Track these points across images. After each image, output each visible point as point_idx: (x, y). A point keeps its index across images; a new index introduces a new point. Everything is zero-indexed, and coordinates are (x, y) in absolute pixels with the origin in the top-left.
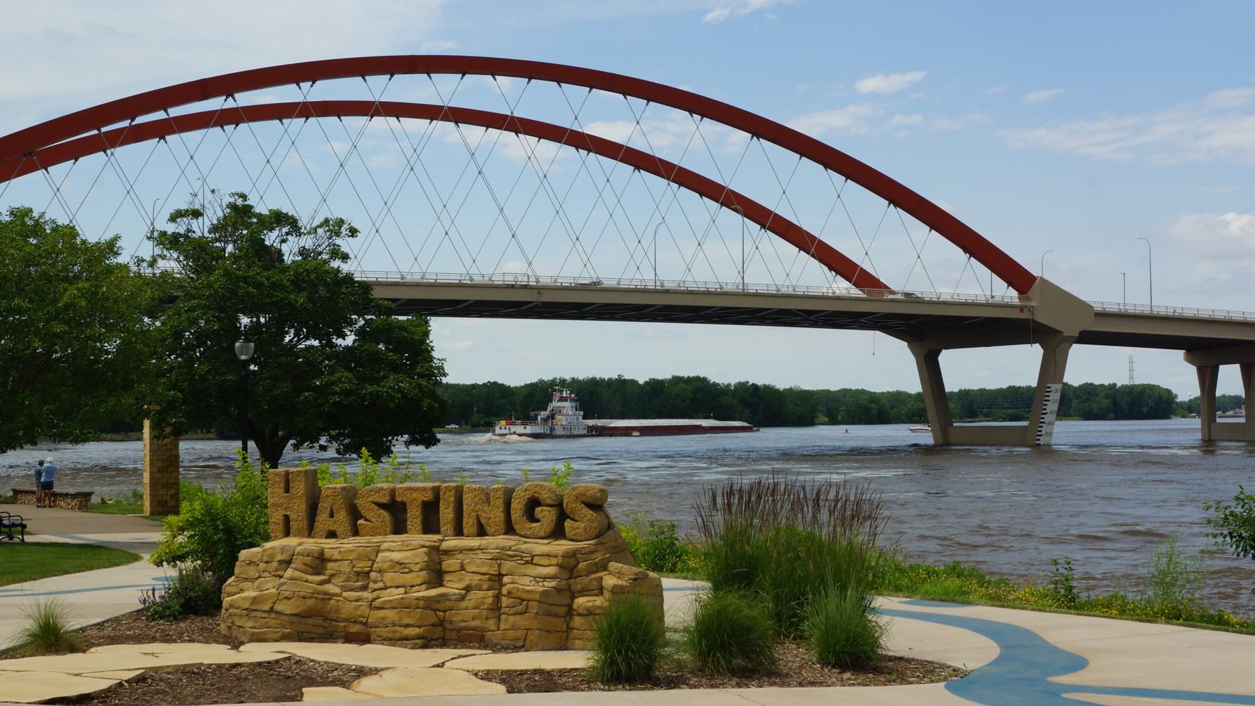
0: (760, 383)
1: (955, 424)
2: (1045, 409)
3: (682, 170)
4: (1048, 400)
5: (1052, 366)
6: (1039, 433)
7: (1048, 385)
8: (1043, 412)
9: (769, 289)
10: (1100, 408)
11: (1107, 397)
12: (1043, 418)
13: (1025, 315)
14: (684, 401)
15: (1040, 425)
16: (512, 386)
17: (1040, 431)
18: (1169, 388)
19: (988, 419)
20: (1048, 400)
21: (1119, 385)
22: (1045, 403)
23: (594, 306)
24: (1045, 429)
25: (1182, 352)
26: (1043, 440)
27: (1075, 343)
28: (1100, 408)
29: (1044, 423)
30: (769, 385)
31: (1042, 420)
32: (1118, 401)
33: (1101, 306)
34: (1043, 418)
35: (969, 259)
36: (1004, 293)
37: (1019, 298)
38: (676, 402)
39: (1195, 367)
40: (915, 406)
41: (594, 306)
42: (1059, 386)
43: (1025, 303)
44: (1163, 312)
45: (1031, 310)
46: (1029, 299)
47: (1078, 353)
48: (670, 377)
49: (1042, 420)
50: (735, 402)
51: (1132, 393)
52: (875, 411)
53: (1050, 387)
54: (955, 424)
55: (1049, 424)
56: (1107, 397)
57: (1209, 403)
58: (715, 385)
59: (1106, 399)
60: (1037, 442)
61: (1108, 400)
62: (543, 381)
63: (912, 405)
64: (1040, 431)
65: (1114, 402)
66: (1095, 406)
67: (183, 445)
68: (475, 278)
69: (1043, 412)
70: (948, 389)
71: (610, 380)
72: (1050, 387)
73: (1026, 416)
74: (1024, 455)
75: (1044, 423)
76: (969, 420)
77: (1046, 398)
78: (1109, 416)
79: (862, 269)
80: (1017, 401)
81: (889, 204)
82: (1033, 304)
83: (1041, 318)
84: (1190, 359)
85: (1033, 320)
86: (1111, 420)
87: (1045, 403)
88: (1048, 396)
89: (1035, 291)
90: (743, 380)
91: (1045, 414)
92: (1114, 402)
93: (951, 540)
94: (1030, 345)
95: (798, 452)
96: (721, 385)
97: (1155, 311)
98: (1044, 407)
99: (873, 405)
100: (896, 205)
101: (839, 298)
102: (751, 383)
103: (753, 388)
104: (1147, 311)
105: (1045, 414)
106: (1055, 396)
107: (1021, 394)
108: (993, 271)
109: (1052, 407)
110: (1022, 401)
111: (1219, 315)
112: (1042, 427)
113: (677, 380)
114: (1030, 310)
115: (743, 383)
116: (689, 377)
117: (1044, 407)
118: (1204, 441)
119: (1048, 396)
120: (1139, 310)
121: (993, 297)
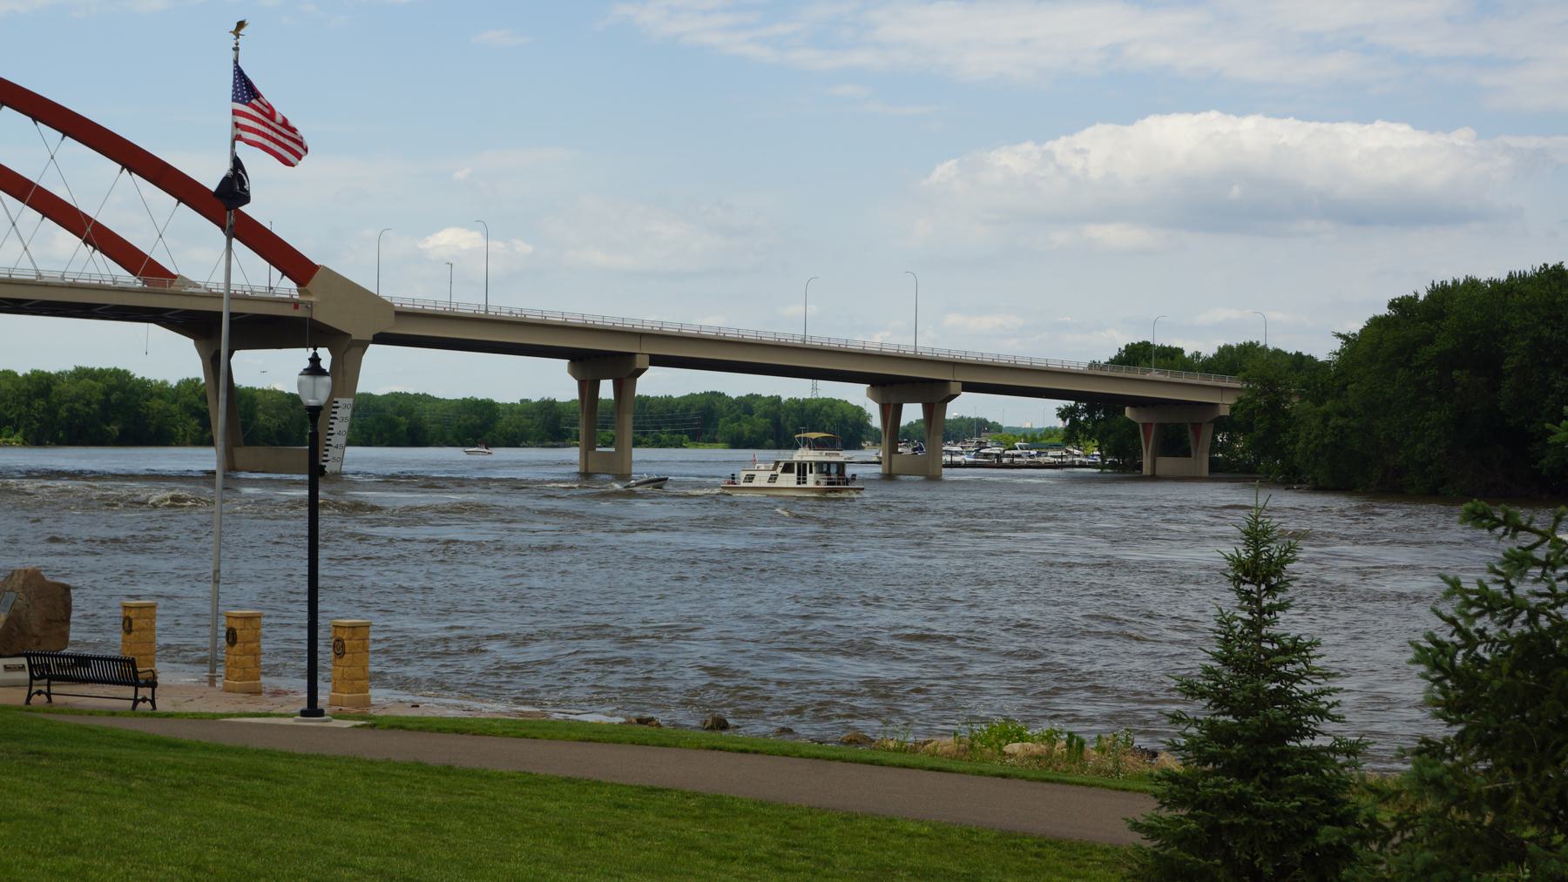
1: (597, 449)
3: (98, 228)
4: (335, 418)
5: (345, 372)
8: (330, 432)
10: (753, 432)
11: (765, 415)
14: (88, 404)
16: (52, 372)
17: (326, 456)
18: (121, 368)
20: (335, 418)
21: (785, 398)
24: (332, 453)
25: (566, 362)
27: (373, 343)
28: (753, 432)
29: (330, 445)
32: (782, 421)
36: (286, 287)
38: (77, 405)
39: (576, 382)
40: (468, 422)
42: (350, 401)
43: (305, 298)
44: (505, 314)
45: (310, 306)
46: (308, 293)
48: (72, 368)
50: (175, 408)
51: (803, 410)
52: (404, 428)
56: (765, 415)
57: (894, 432)
58: (143, 384)
59: (766, 418)
61: (767, 420)
62: (119, 370)
63: (465, 420)
64: (326, 456)
65: (777, 423)
66: (746, 428)
67: (638, 454)
69: (330, 432)
74: (918, 482)
75: (330, 445)
76: (551, 443)
77: (333, 415)
78: (767, 443)
79: (151, 260)
80: (645, 418)
81: (122, 169)
82: (313, 299)
83: (323, 316)
84: (573, 371)
85: (311, 320)
86: (769, 448)
91: (332, 434)
92: (777, 423)
93: (830, 635)
99: (402, 419)
100: (130, 171)
101: (123, 290)
105: (332, 434)
106: (344, 411)
107: (650, 407)
108: (272, 262)
109: (341, 425)
110: (651, 418)
111: (534, 316)
113: (82, 374)
115: (1410, 298)
116: (101, 370)
121: (271, 288)
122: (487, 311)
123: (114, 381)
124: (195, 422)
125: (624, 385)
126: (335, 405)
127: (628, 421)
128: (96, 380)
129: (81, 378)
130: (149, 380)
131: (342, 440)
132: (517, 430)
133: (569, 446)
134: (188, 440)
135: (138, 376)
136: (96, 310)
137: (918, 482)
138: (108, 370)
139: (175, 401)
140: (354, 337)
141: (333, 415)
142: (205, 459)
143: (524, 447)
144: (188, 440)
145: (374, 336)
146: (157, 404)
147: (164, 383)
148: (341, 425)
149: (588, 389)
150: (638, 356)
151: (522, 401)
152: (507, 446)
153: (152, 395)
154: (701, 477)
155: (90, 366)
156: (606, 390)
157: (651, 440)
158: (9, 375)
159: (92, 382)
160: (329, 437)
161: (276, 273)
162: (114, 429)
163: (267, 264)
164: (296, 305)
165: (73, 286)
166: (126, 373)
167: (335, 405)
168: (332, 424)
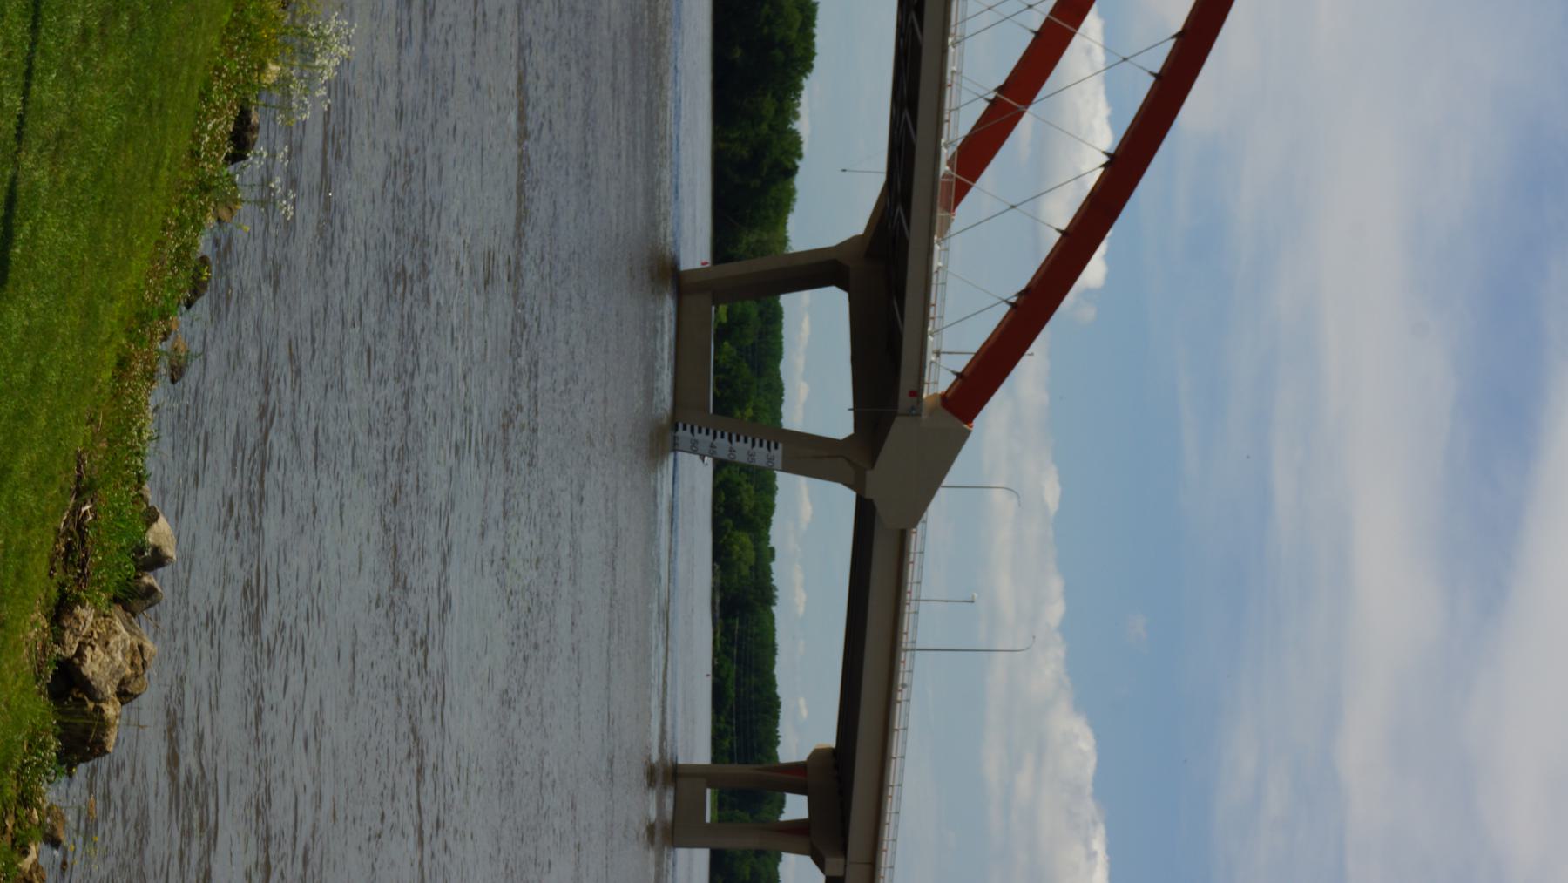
0: (800, 181)
1: (709, 791)
2: (738, 440)
4: (753, 445)
6: (696, 429)
7: (780, 445)
9: (940, 287)
12: (722, 436)
13: (904, 400)
15: (711, 431)
18: (817, 61)
19: (718, 645)
20: (753, 445)
22: (750, 439)
23: (904, 222)
24: (704, 439)
26: (684, 435)
30: (794, 200)
31: (719, 434)
33: (896, 783)
34: (722, 436)
35: (1006, 301)
36: (940, 378)
37: (935, 395)
40: (746, 497)
41: (904, 222)
45: (915, 410)
47: (842, 500)
49: (719, 434)
53: (776, 447)
54: (709, 791)
55: (712, 446)
58: (798, 88)
60: (681, 425)
62: (812, 58)
68: (905, 690)
70: (787, 301)
71: (777, 732)
72: (776, 447)
73: (722, 719)
74: (650, 393)
76: (718, 600)
77: (757, 442)
82: (924, 416)
83: (899, 431)
84: (818, 754)
85: (895, 415)
87: (750, 439)
88: (761, 445)
89: (950, 421)
90: (805, 148)
94: (851, 406)
95: (675, 513)
96: (796, 102)
97: (905, 657)
98: (742, 438)
102: (799, 163)
103: (789, 165)
104: (906, 640)
105: (730, 440)
106: (761, 456)
109: (742, 451)
112: (707, 433)
114: (913, 408)
116: (813, 36)
117: (742, 438)
118: (676, 767)
119: (761, 445)
120: (908, 623)
121: (938, 353)
122: (906, 650)
123: (799, 52)
124: (745, 153)
125: (799, 836)
126: (772, 444)
127: (750, 842)
128: (800, 30)
129: (802, 11)
130: (800, 96)
131: (723, 454)
132: (735, 557)
133: (714, 624)
134: (722, 145)
135: (805, 82)
136: (906, 114)
137: (650, 393)
138: (813, 45)
139: (771, 127)
140: (869, 473)
141: (757, 442)
142: (695, 251)
143: (713, 568)
144: (722, 145)
145: (870, 502)
146: (768, 105)
147: (796, 116)
148: (742, 451)
149: (796, 777)
150: (841, 860)
151: (772, 550)
152: (717, 489)
153: (780, 100)
154: (673, 509)
155: (818, 22)
156: (796, 807)
157: (722, 726)
158: (808, 15)
159: (797, 25)
160: (726, 435)
161: (961, 364)
162: (738, 53)
163: (975, 348)
164: (916, 394)
165: (941, 86)
166: (809, 67)
167: (772, 444)
168: (746, 441)
